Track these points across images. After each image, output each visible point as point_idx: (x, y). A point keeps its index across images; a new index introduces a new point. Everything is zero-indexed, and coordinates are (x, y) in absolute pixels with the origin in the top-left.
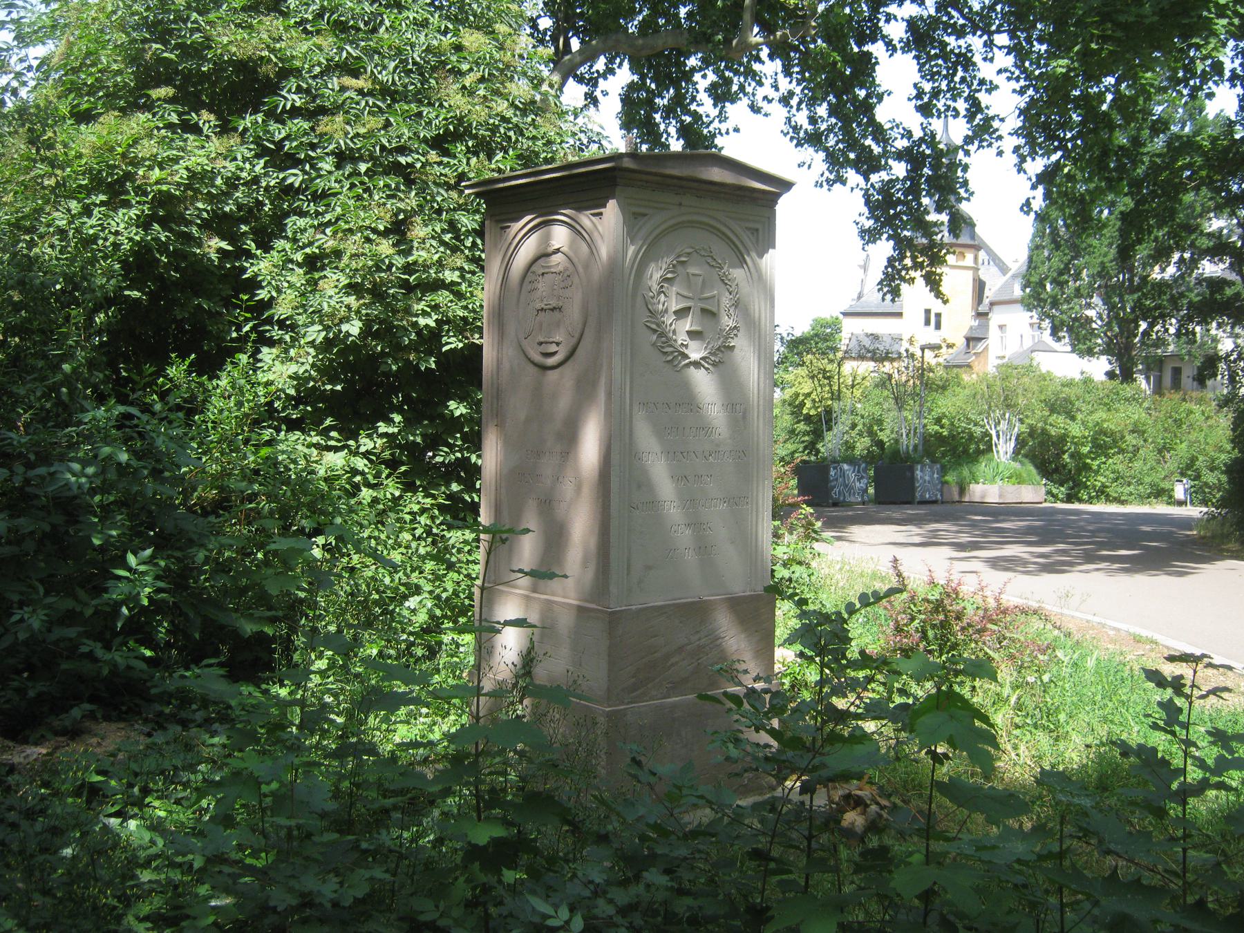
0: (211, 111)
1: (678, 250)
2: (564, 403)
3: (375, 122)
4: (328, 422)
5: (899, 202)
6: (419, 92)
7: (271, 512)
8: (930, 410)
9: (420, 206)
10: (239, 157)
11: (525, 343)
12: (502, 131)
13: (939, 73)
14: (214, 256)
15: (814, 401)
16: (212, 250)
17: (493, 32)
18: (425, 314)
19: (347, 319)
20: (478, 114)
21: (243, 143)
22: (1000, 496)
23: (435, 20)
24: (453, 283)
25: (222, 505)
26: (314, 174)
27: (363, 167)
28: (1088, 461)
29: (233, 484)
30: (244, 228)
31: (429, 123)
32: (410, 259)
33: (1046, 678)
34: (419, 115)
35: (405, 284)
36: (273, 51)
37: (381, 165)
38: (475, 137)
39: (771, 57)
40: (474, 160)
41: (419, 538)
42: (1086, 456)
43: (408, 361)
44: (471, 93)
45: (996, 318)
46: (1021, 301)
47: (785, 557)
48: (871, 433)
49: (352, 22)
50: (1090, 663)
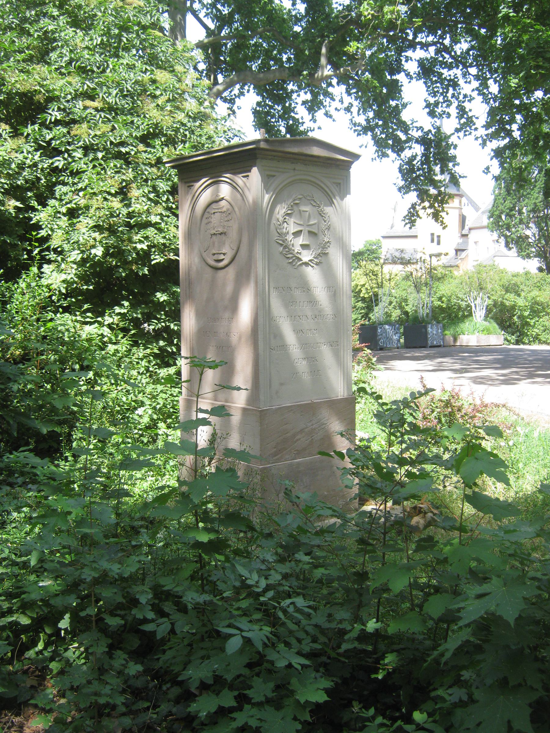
0: (6, 124)
1: (294, 196)
2: (229, 289)
3: (105, 128)
4: (86, 306)
6: (132, 109)
7: (55, 361)
8: (436, 293)
9: (134, 177)
10: (25, 151)
11: (204, 255)
12: (182, 131)
13: (438, 92)
14: (12, 211)
15: (367, 289)
16: (11, 208)
17: (173, 71)
18: (140, 242)
19: (93, 247)
20: (166, 122)
21: (27, 142)
22: (478, 342)
23: (139, 64)
24: (157, 223)
25: (25, 358)
26: (70, 160)
27: (100, 155)
29: (31, 345)
30: (30, 194)
31: (138, 128)
32: (130, 210)
33: (511, 443)
34: (132, 122)
35: (128, 225)
36: (42, 86)
37: (110, 153)
38: (166, 135)
39: (338, 84)
40: (166, 149)
41: (142, 373)
42: (527, 317)
43: (132, 270)
44: (162, 109)
45: (473, 236)
46: (487, 227)
47: (356, 379)
48: (401, 307)
49: (89, 68)
50: (536, 434)
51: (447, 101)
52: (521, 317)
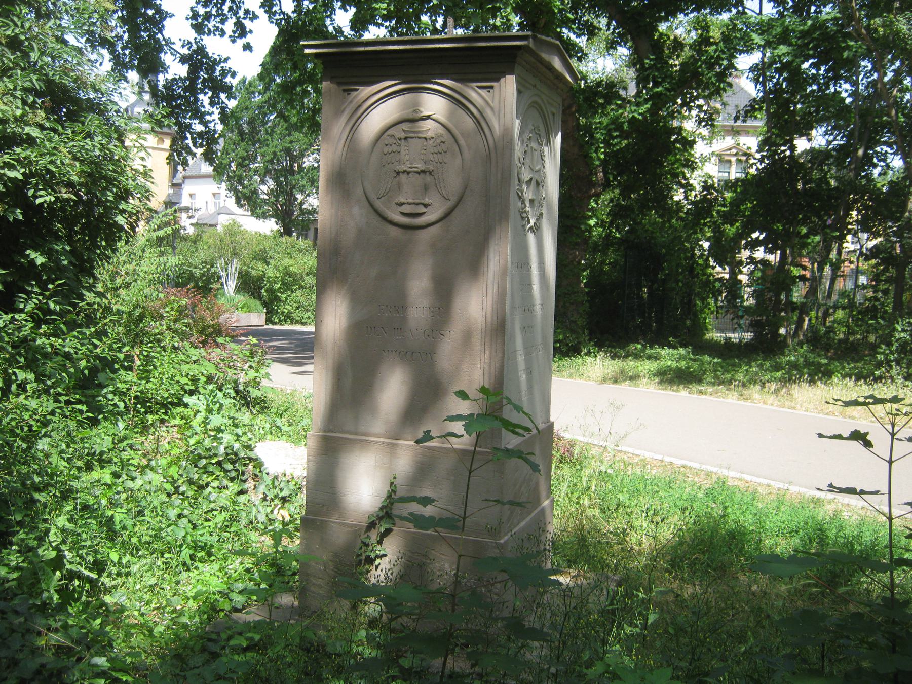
5: (180, 96)
52: (270, 291)
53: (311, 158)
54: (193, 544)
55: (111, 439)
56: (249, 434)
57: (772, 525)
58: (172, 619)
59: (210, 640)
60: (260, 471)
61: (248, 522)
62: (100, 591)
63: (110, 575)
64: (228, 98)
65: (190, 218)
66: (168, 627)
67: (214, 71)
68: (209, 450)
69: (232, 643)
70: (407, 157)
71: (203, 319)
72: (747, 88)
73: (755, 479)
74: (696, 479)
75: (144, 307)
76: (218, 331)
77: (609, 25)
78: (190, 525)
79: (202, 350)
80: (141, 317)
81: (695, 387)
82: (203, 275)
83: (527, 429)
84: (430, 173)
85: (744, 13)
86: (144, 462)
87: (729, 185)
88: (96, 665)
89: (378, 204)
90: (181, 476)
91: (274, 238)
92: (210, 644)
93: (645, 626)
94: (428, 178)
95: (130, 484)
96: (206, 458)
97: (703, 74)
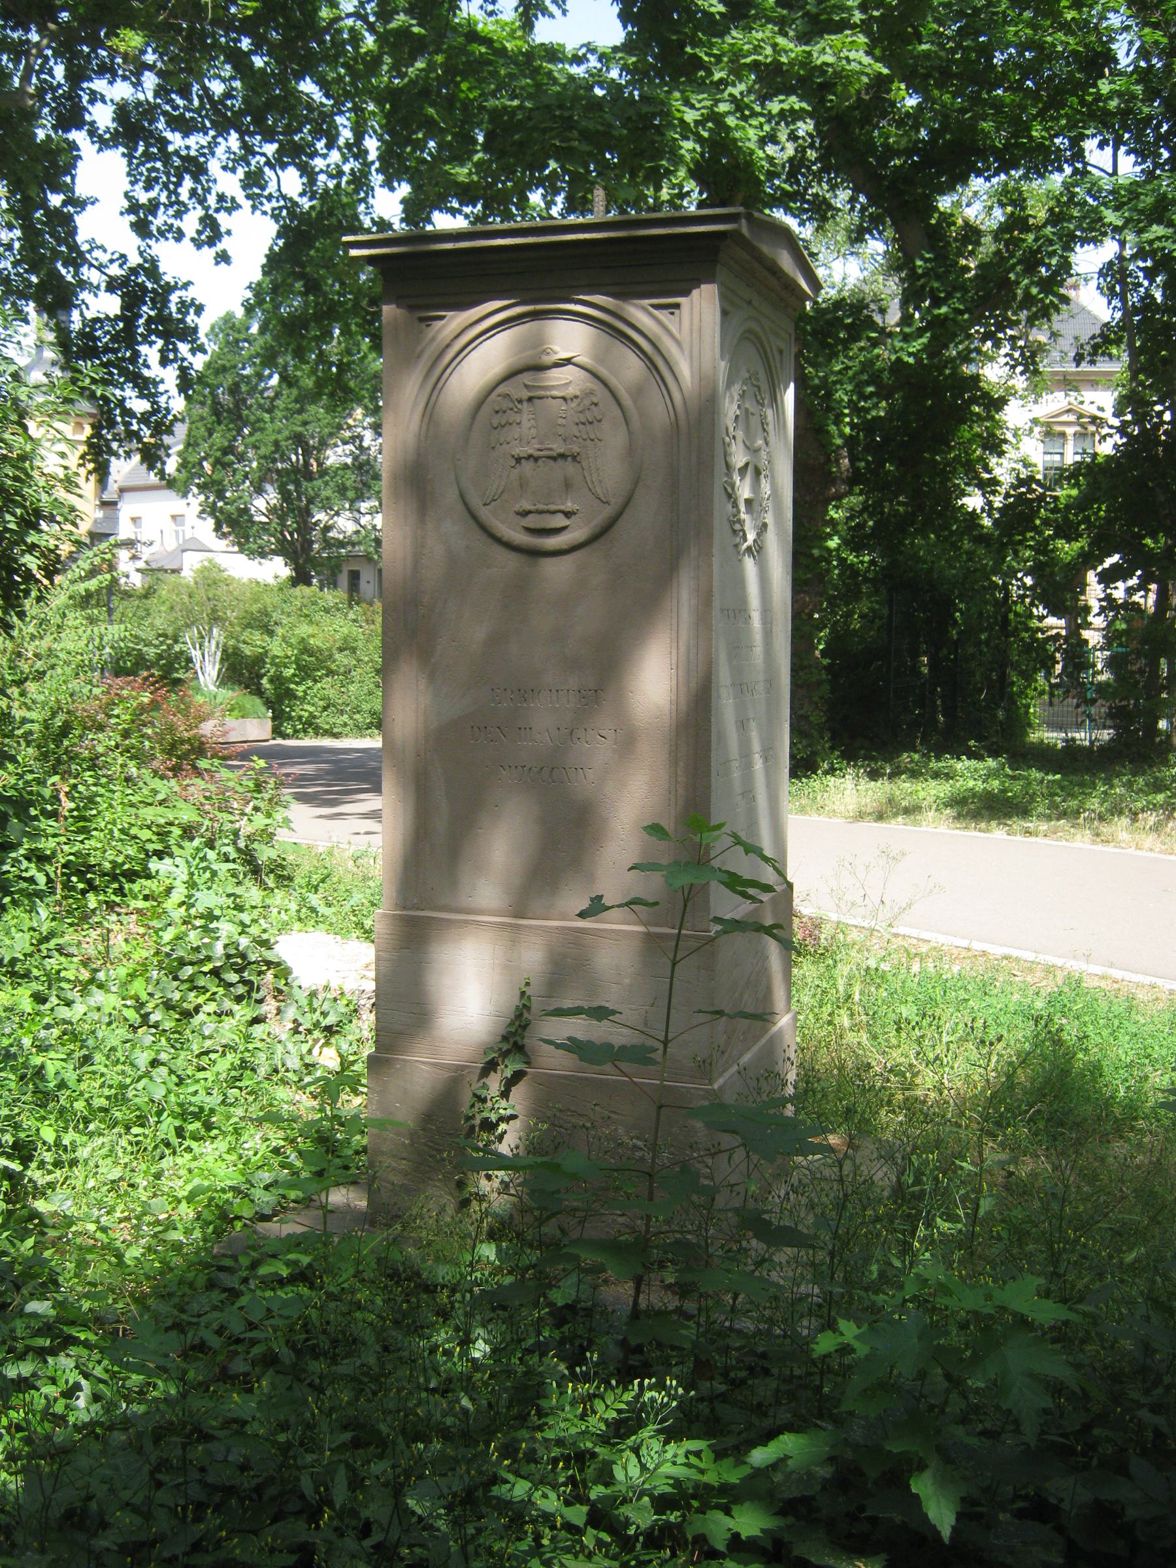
13: (156, 180)
28: (292, 686)
42: (290, 680)
51: (178, 202)
52: (277, 680)
53: (339, 450)
54: (178, 1110)
55: (27, 936)
56: (262, 921)
57: (1164, 1052)
58: (155, 1236)
59: (221, 1269)
60: (286, 984)
61: (269, 1070)
62: (27, 1194)
63: (42, 1165)
64: (193, 351)
65: (134, 558)
66: (149, 1249)
67: (166, 302)
68: (197, 949)
69: (263, 1271)
70: (533, 431)
71: (171, 728)
72: (1093, 305)
73: (1128, 976)
74: (1029, 979)
75: (68, 712)
76: (200, 749)
77: (852, 200)
78: (174, 1077)
79: (173, 782)
80: (65, 730)
81: (1018, 824)
82: (160, 657)
83: (767, 888)
84: (574, 458)
85: (1085, 173)
86: (85, 975)
87: (1062, 475)
88: (34, 1315)
89: (484, 513)
90: (151, 995)
91: (281, 589)
92: (222, 1275)
93: (973, 1218)
94: (570, 467)
95: (63, 1012)
96: (192, 964)
97: (1017, 283)
